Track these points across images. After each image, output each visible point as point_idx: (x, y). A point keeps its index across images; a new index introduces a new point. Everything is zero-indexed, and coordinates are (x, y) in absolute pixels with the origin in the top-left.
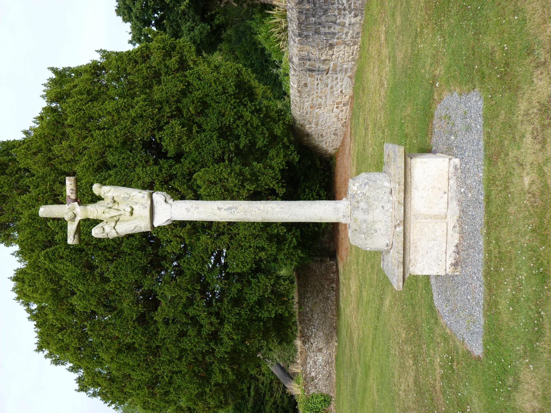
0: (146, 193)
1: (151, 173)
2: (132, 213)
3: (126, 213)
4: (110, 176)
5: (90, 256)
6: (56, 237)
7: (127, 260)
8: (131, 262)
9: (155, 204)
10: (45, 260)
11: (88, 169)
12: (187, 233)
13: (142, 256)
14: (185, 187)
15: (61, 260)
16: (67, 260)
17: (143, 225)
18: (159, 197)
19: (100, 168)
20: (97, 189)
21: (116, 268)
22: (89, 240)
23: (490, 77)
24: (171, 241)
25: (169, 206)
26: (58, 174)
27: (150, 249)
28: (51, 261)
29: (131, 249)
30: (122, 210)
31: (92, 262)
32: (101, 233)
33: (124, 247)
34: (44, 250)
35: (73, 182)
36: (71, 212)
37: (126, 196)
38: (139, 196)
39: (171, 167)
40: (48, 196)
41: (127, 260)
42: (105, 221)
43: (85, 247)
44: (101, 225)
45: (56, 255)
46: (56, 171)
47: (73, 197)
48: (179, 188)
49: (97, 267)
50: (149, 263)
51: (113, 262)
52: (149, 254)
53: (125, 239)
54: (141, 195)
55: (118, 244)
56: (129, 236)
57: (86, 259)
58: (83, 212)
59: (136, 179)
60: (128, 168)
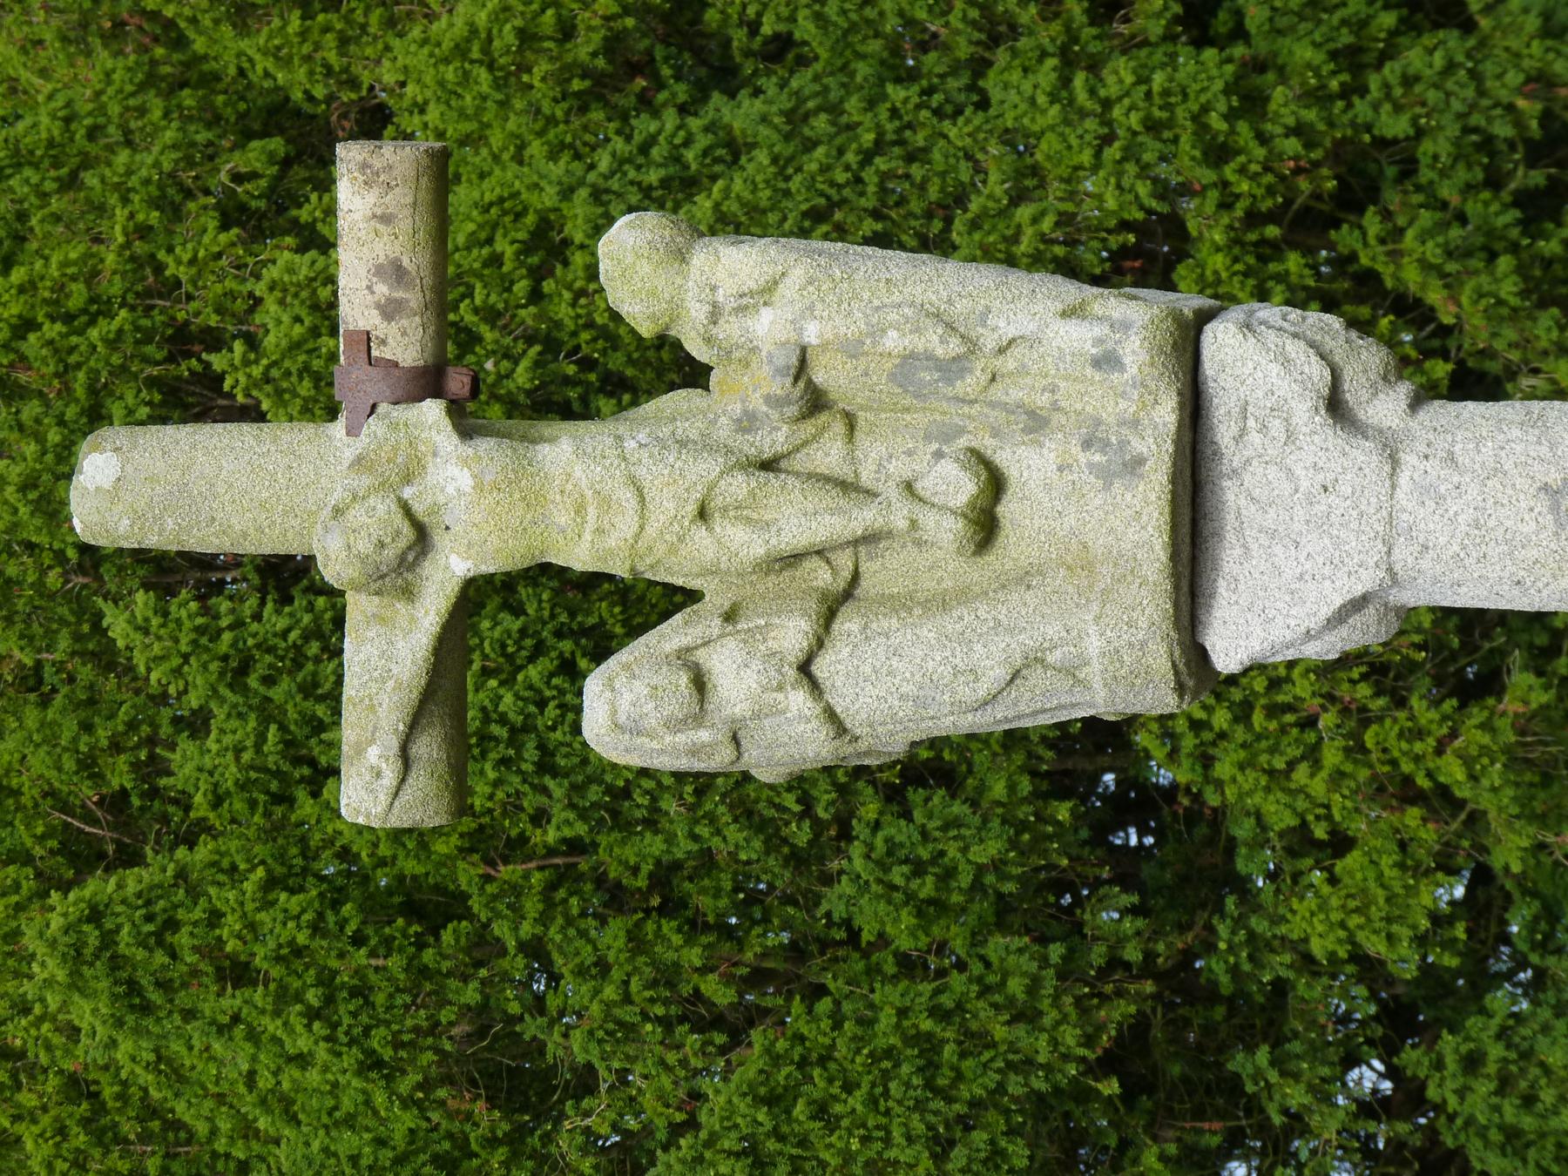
0: (1132, 319)
1: (1152, 127)
2: (984, 526)
3: (929, 519)
4: (734, 150)
5: (517, 965)
6: (187, 763)
7: (887, 1019)
8: (928, 1046)
9: (1224, 431)
10: (77, 984)
11: (509, 80)
12: (1515, 760)
13: (1033, 988)
14: (1509, 288)
15: (232, 1001)
16: (284, 998)
17: (1094, 645)
18: (1264, 361)
19: (634, 69)
20: (640, 269)
21: (776, 1101)
22: (513, 806)
23: (21, 202)
24: (1341, 843)
25: (1364, 454)
26: (215, 120)
27: (1109, 916)
28: (133, 1001)
29: (931, 910)
30: (892, 492)
31: (531, 1028)
32: (676, 725)
33: (856, 894)
34: (65, 887)
35: (401, 198)
36: (374, 496)
37: (933, 341)
38: (1075, 346)
39: (1354, 59)
40: (114, 343)
41: (887, 1019)
42: (716, 599)
43: (467, 874)
44: (671, 635)
45: (183, 939)
46: (188, 98)
47: (405, 345)
48: (1435, 296)
49: (585, 1082)
50: (1107, 1064)
51: (737, 1037)
52: (1115, 963)
53: (870, 809)
54: (1079, 337)
55: (797, 859)
56: (934, 768)
57: (471, 994)
58: (492, 500)
59: (996, 185)
60: (912, 76)
